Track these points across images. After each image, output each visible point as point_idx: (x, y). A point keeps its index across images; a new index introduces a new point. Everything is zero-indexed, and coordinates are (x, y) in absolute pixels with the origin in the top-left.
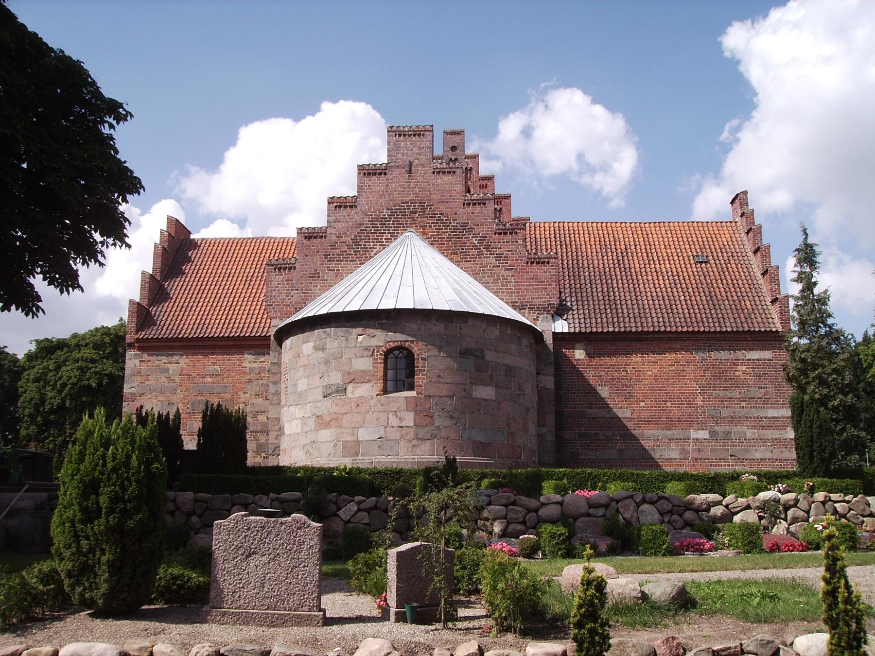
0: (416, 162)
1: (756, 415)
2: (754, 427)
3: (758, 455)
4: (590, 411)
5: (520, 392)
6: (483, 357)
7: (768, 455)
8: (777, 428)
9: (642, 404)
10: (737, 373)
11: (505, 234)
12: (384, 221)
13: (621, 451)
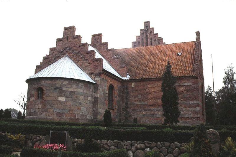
0: (69, 36)
1: (186, 103)
2: (185, 107)
3: (186, 116)
4: (135, 103)
5: (55, 100)
6: (62, 89)
7: (190, 116)
8: (193, 107)
9: (150, 100)
10: (180, 90)
11: (89, 53)
12: (61, 53)
13: (144, 115)
